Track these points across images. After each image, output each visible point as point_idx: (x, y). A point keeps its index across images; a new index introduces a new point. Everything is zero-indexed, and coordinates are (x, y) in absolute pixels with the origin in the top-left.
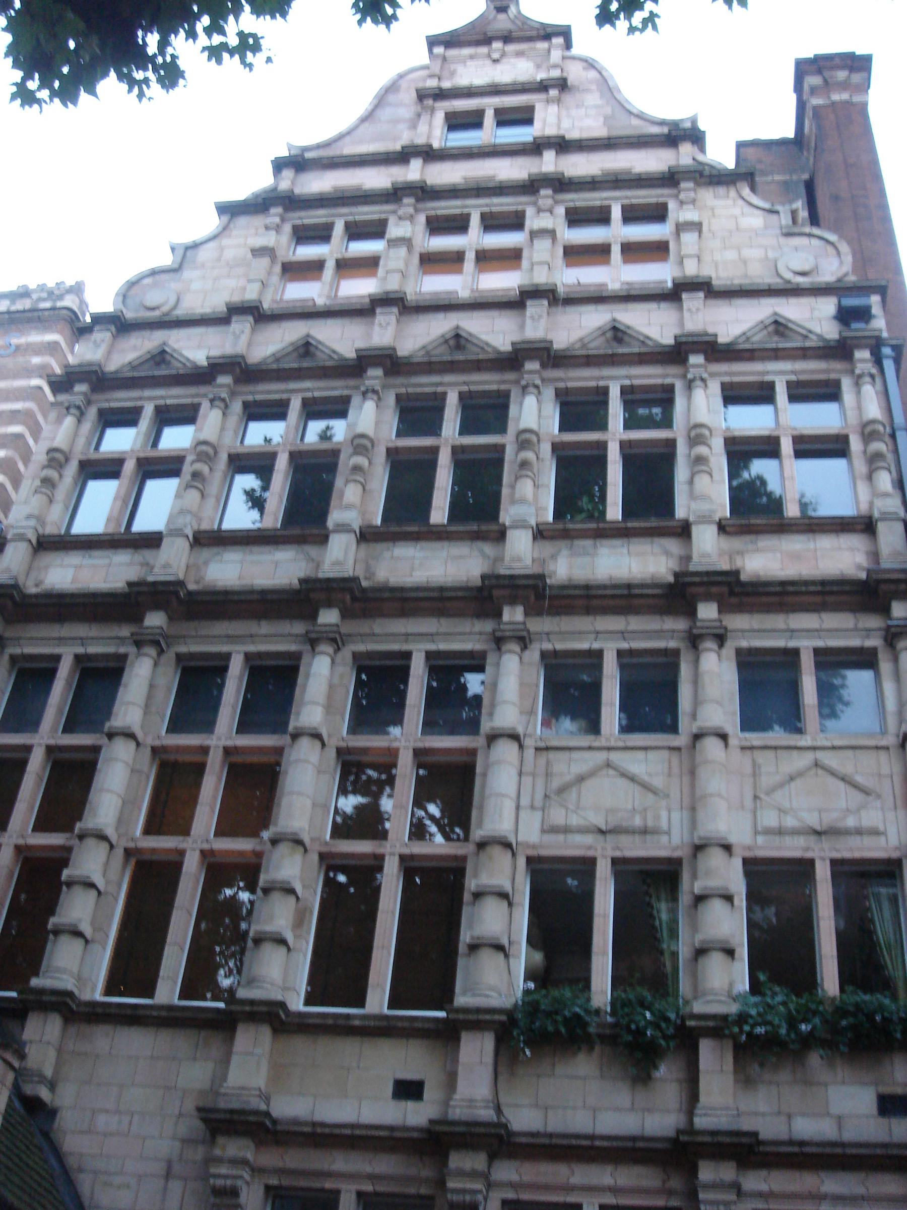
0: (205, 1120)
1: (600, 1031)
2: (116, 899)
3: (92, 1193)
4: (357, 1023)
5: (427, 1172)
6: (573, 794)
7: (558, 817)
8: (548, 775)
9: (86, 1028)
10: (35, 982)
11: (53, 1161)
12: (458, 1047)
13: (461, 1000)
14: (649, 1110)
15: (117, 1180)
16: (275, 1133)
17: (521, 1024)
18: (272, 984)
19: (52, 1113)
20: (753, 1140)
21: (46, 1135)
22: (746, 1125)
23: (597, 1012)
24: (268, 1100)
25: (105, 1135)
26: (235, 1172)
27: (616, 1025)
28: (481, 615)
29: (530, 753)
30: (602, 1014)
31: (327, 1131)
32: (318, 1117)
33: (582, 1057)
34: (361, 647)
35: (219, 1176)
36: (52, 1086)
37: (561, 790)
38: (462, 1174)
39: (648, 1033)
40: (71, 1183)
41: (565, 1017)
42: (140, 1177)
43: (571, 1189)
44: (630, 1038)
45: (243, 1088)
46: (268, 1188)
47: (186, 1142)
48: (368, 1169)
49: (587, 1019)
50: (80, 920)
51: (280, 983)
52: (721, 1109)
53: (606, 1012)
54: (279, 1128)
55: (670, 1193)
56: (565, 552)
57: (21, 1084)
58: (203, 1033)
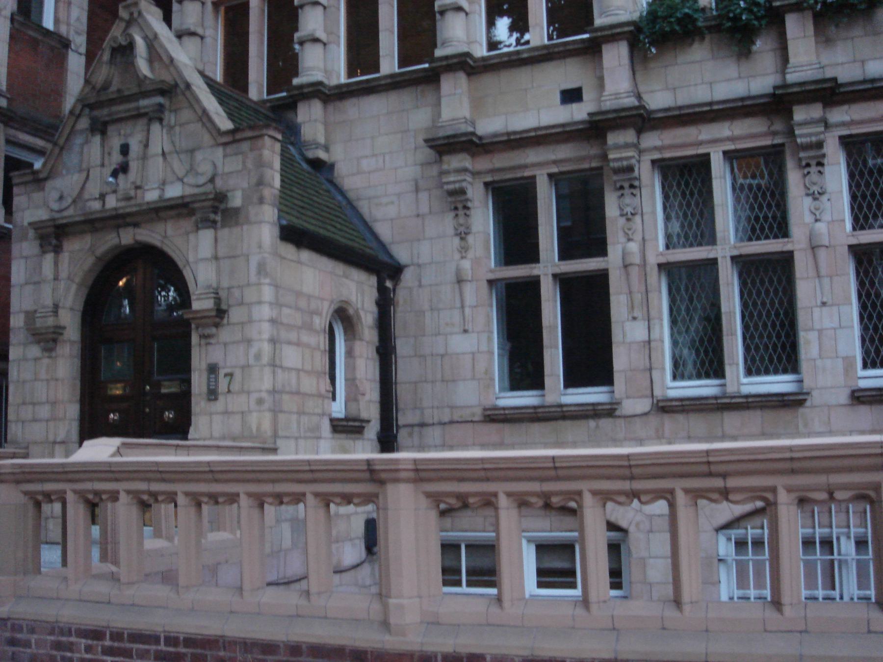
0: (431, 147)
1: (708, 24)
2: (339, 9)
3: (370, 212)
4: (525, 55)
5: (594, 151)
9: (338, 104)
10: (296, 81)
11: (340, 198)
12: (601, 57)
13: (598, 22)
14: (751, 76)
15: (384, 200)
16: (483, 145)
17: (645, 30)
18: (459, 42)
19: (332, 167)
20: (834, 84)
21: (331, 182)
22: (829, 74)
23: (703, 10)
24: (473, 123)
25: (369, 173)
26: (459, 178)
27: (719, 16)
30: (707, 11)
31: (518, 136)
32: (511, 128)
33: (696, 45)
35: (448, 183)
36: (327, 149)
38: (618, 147)
39: (744, 18)
40: (354, 208)
41: (678, 19)
42: (399, 195)
43: (701, 143)
44: (729, 24)
45: (453, 120)
46: (486, 185)
47: (425, 164)
48: (553, 157)
49: (696, 16)
50: (315, 30)
51: (465, 39)
52: (806, 65)
53: (711, 9)
54: (485, 141)
55: (774, 134)
57: (305, 152)
58: (419, 88)
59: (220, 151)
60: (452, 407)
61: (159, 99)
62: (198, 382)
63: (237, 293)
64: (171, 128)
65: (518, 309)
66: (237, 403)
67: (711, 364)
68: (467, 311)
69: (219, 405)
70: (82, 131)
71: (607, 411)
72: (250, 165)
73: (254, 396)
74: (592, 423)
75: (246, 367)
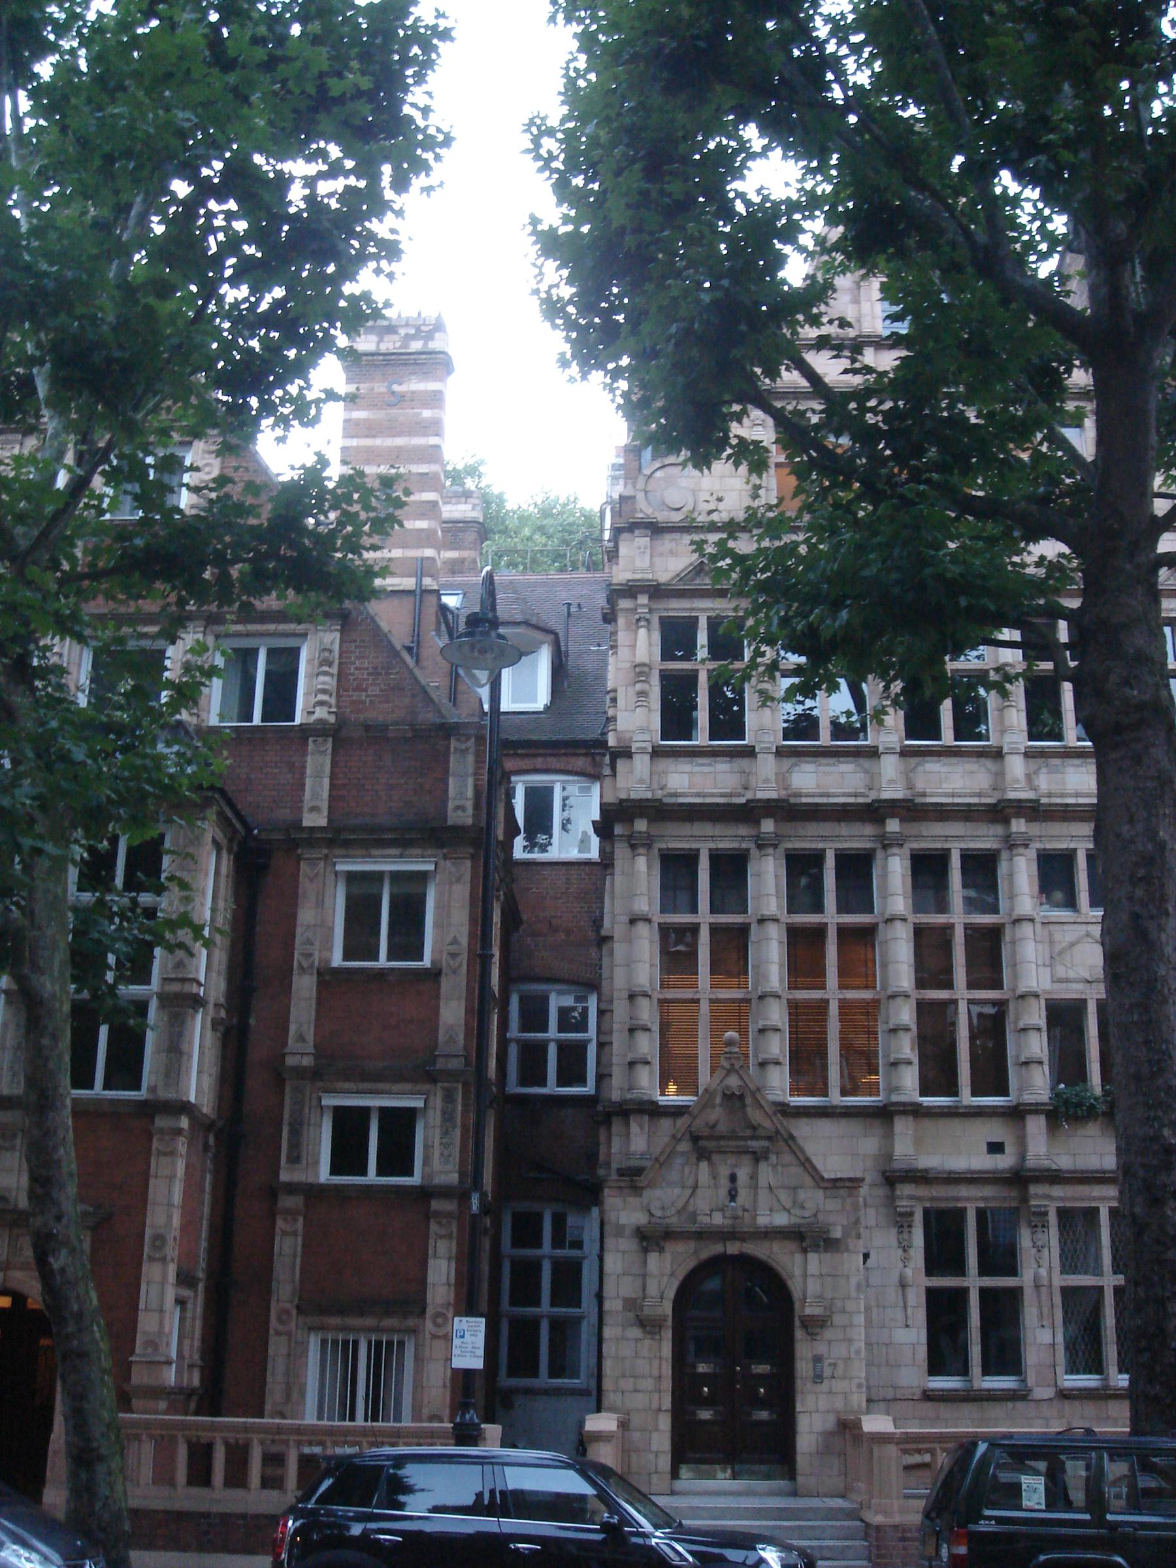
6: (1068, 957)
7: (1061, 972)
8: (1051, 942)
28: (994, 821)
29: (1038, 926)
34: (915, 846)
37: (1060, 953)
56: (1044, 770)
59: (821, 1192)
60: (895, 1388)
61: (766, 1143)
62: (803, 1368)
63: (839, 1304)
64: (774, 1167)
65: (944, 1312)
66: (839, 1386)
67: (1095, 1365)
68: (909, 1311)
69: (824, 1387)
70: (682, 1154)
71: (1019, 1396)
72: (848, 1207)
73: (856, 1381)
74: (1010, 1404)
75: (848, 1359)
